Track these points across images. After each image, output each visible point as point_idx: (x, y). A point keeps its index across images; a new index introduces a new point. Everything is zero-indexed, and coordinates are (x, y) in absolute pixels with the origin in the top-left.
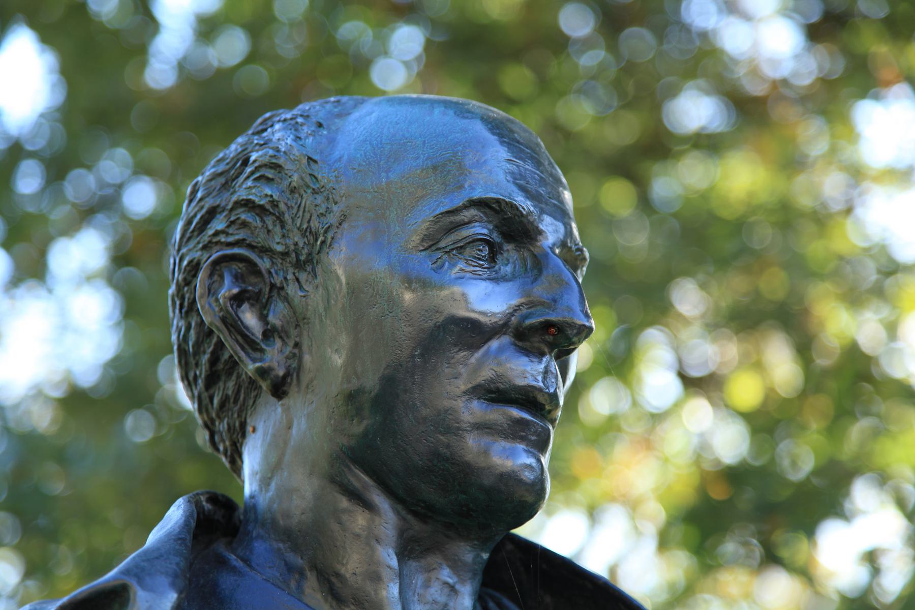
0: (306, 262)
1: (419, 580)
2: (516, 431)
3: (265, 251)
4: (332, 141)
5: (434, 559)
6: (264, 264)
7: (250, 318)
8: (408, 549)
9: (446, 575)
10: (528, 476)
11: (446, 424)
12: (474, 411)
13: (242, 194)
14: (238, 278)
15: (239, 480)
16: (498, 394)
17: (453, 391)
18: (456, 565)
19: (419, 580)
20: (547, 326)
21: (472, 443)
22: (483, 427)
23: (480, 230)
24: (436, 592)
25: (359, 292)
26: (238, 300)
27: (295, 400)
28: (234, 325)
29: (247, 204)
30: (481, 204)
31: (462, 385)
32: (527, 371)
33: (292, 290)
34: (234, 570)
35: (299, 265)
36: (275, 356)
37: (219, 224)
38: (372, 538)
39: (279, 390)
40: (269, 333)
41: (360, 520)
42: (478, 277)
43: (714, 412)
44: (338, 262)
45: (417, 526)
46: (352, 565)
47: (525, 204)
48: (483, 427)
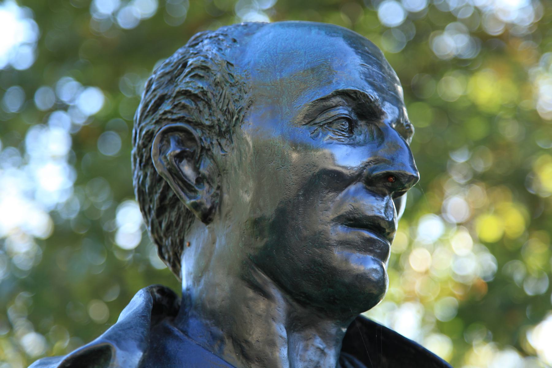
0: (226, 132)
1: (300, 345)
2: (367, 246)
3: (198, 125)
5: (310, 332)
6: (197, 133)
7: (187, 170)
8: (294, 325)
9: (318, 342)
12: (339, 232)
14: (179, 143)
16: (355, 221)
17: (326, 216)
18: (324, 336)
19: (300, 345)
20: (388, 176)
21: (337, 255)
23: (343, 111)
24: (311, 354)
26: (180, 157)
27: (218, 225)
29: (186, 94)
30: (344, 94)
32: (374, 206)
33: (216, 151)
35: (221, 134)
37: (166, 107)
38: (269, 317)
40: (200, 180)
41: (261, 305)
44: (248, 133)
45: (299, 309)
46: (255, 335)
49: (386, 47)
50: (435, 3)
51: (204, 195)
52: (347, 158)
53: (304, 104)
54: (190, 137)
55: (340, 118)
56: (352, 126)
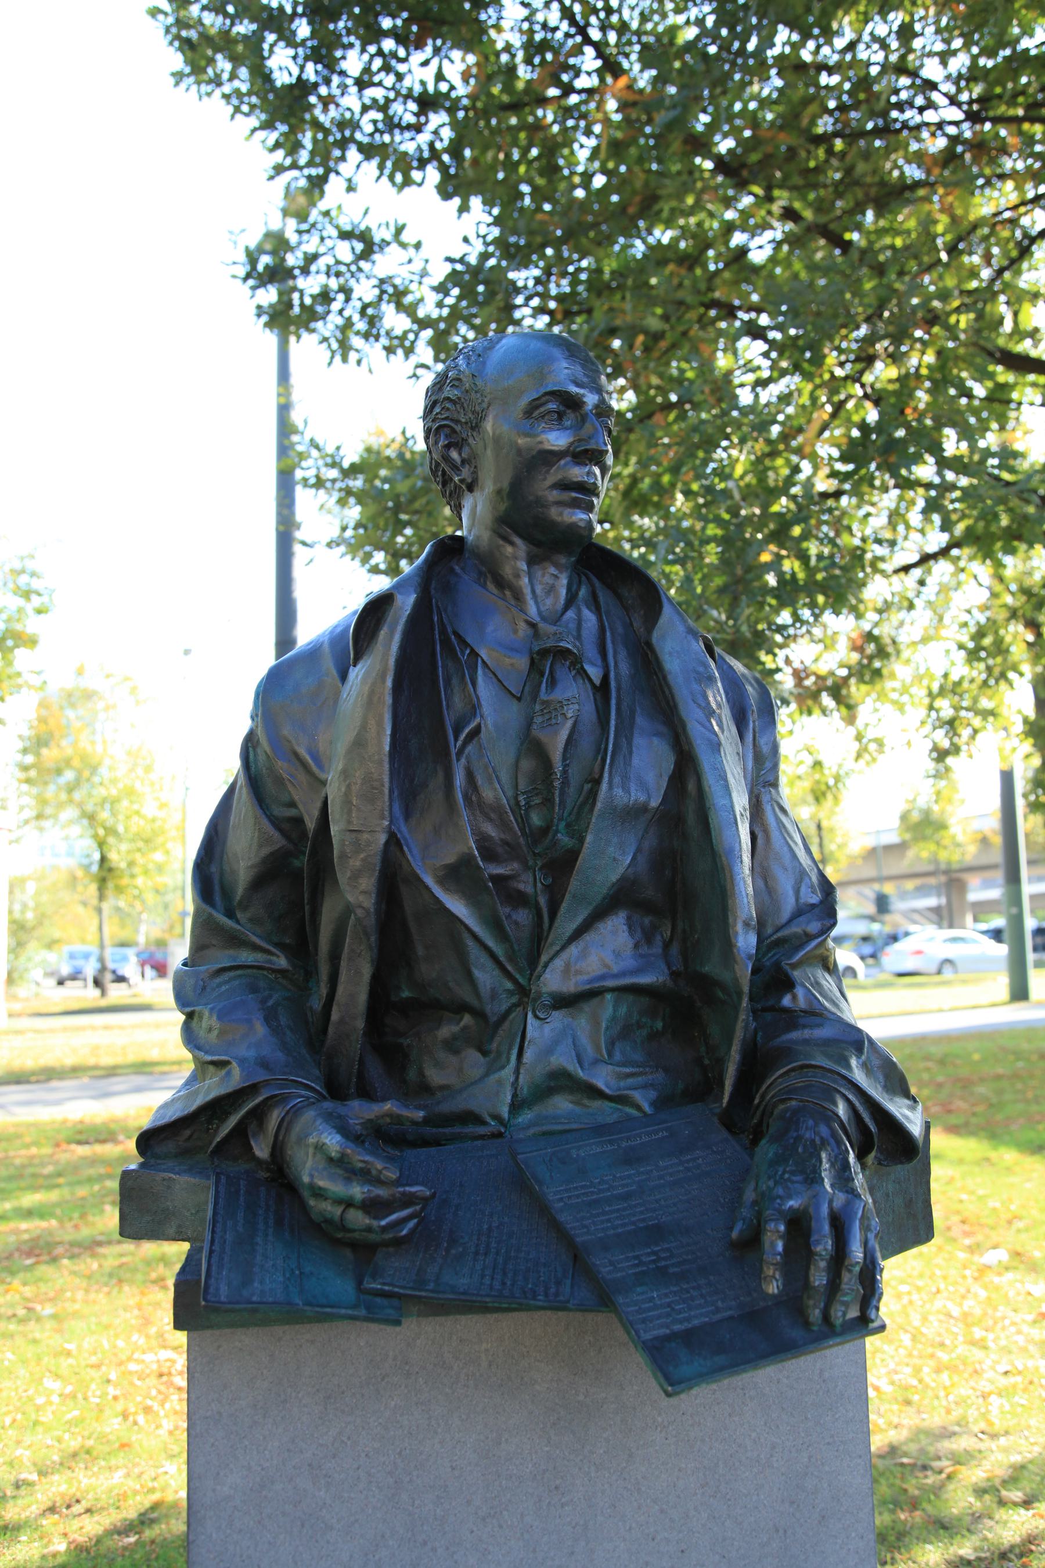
0: (476, 427)
1: (539, 573)
2: (575, 504)
3: (457, 422)
4: (484, 363)
5: (547, 564)
6: (458, 428)
7: (454, 455)
8: (532, 561)
9: (552, 570)
10: (582, 524)
11: (540, 502)
12: (555, 495)
13: (446, 394)
14: (447, 436)
15: (260, 732)
16: (566, 486)
17: (544, 487)
18: (556, 565)
19: (539, 573)
20: (586, 451)
21: (554, 513)
22: (559, 503)
23: (552, 406)
24: (548, 579)
25: (497, 440)
26: (448, 447)
27: (477, 494)
28: (446, 459)
29: (448, 399)
30: (552, 393)
31: (551, 479)
32: (578, 473)
33: (471, 440)
34: (457, 575)
35: (473, 428)
36: (466, 472)
37: (437, 410)
38: (515, 556)
39: (471, 488)
40: (463, 462)
41: (509, 549)
42: (551, 430)
43: (150, 1109)
44: (488, 426)
45: (535, 550)
46: (507, 571)
47: (574, 389)
48: (559, 503)
49: (843, 267)
50: (1040, 303)
51: (466, 472)
52: (557, 439)
53: (524, 402)
54: (454, 431)
55: (550, 412)
56: (560, 416)
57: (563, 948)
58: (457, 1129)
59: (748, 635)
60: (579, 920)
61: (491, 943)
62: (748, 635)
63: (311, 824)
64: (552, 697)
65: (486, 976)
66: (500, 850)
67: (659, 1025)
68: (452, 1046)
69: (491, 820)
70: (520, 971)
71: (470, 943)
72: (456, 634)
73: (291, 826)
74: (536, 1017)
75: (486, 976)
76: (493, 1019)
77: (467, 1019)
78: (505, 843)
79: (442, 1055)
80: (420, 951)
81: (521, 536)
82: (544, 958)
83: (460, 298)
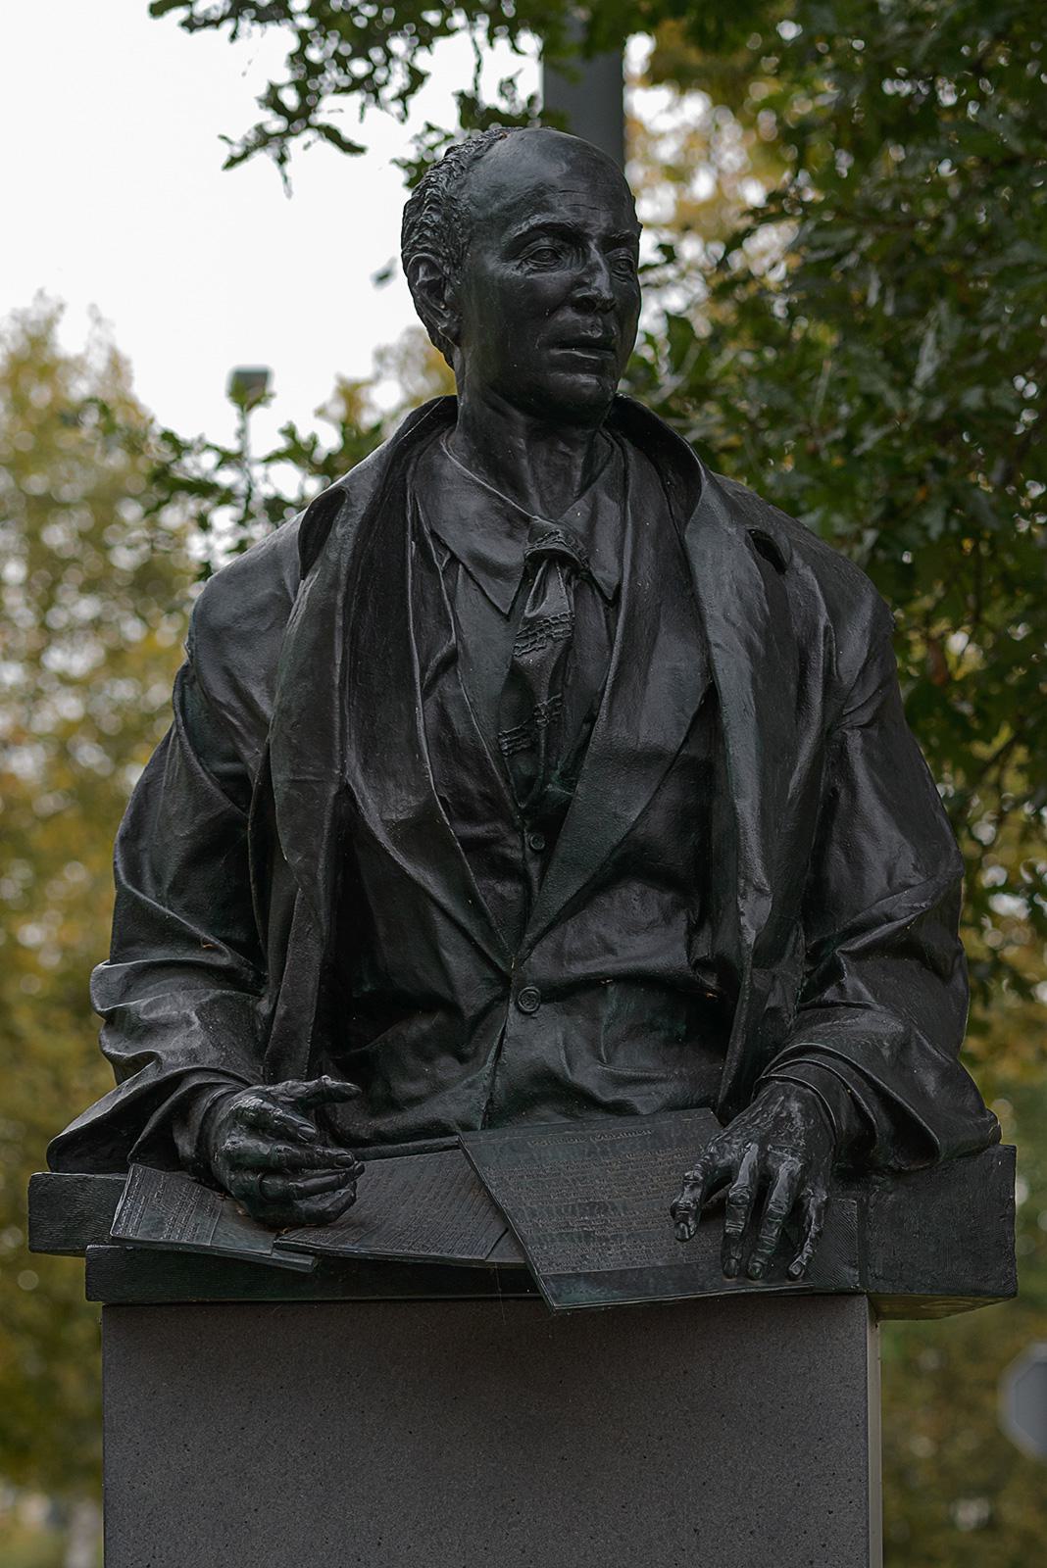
57: (551, 927)
58: (593, 585)
59: (821, 955)
60: (572, 891)
61: (462, 919)
62: (821, 955)
63: (255, 782)
64: (542, 608)
65: (459, 963)
66: (479, 807)
67: (682, 1028)
68: (424, 1051)
69: (467, 769)
70: (501, 953)
71: (438, 918)
72: (433, 534)
73: (236, 784)
74: (519, 1010)
75: (459, 963)
76: (469, 1014)
77: (439, 1017)
78: (484, 796)
79: (411, 1062)
80: (382, 930)
81: (517, 406)
82: (529, 937)
83: (895, 76)
